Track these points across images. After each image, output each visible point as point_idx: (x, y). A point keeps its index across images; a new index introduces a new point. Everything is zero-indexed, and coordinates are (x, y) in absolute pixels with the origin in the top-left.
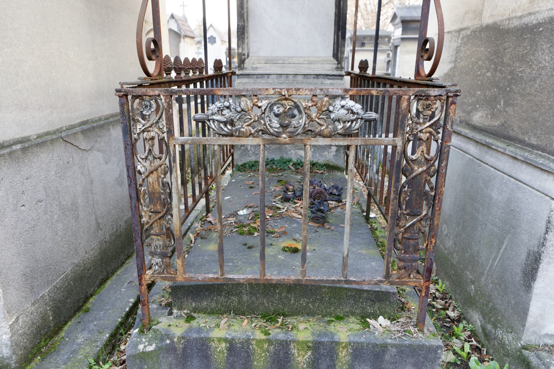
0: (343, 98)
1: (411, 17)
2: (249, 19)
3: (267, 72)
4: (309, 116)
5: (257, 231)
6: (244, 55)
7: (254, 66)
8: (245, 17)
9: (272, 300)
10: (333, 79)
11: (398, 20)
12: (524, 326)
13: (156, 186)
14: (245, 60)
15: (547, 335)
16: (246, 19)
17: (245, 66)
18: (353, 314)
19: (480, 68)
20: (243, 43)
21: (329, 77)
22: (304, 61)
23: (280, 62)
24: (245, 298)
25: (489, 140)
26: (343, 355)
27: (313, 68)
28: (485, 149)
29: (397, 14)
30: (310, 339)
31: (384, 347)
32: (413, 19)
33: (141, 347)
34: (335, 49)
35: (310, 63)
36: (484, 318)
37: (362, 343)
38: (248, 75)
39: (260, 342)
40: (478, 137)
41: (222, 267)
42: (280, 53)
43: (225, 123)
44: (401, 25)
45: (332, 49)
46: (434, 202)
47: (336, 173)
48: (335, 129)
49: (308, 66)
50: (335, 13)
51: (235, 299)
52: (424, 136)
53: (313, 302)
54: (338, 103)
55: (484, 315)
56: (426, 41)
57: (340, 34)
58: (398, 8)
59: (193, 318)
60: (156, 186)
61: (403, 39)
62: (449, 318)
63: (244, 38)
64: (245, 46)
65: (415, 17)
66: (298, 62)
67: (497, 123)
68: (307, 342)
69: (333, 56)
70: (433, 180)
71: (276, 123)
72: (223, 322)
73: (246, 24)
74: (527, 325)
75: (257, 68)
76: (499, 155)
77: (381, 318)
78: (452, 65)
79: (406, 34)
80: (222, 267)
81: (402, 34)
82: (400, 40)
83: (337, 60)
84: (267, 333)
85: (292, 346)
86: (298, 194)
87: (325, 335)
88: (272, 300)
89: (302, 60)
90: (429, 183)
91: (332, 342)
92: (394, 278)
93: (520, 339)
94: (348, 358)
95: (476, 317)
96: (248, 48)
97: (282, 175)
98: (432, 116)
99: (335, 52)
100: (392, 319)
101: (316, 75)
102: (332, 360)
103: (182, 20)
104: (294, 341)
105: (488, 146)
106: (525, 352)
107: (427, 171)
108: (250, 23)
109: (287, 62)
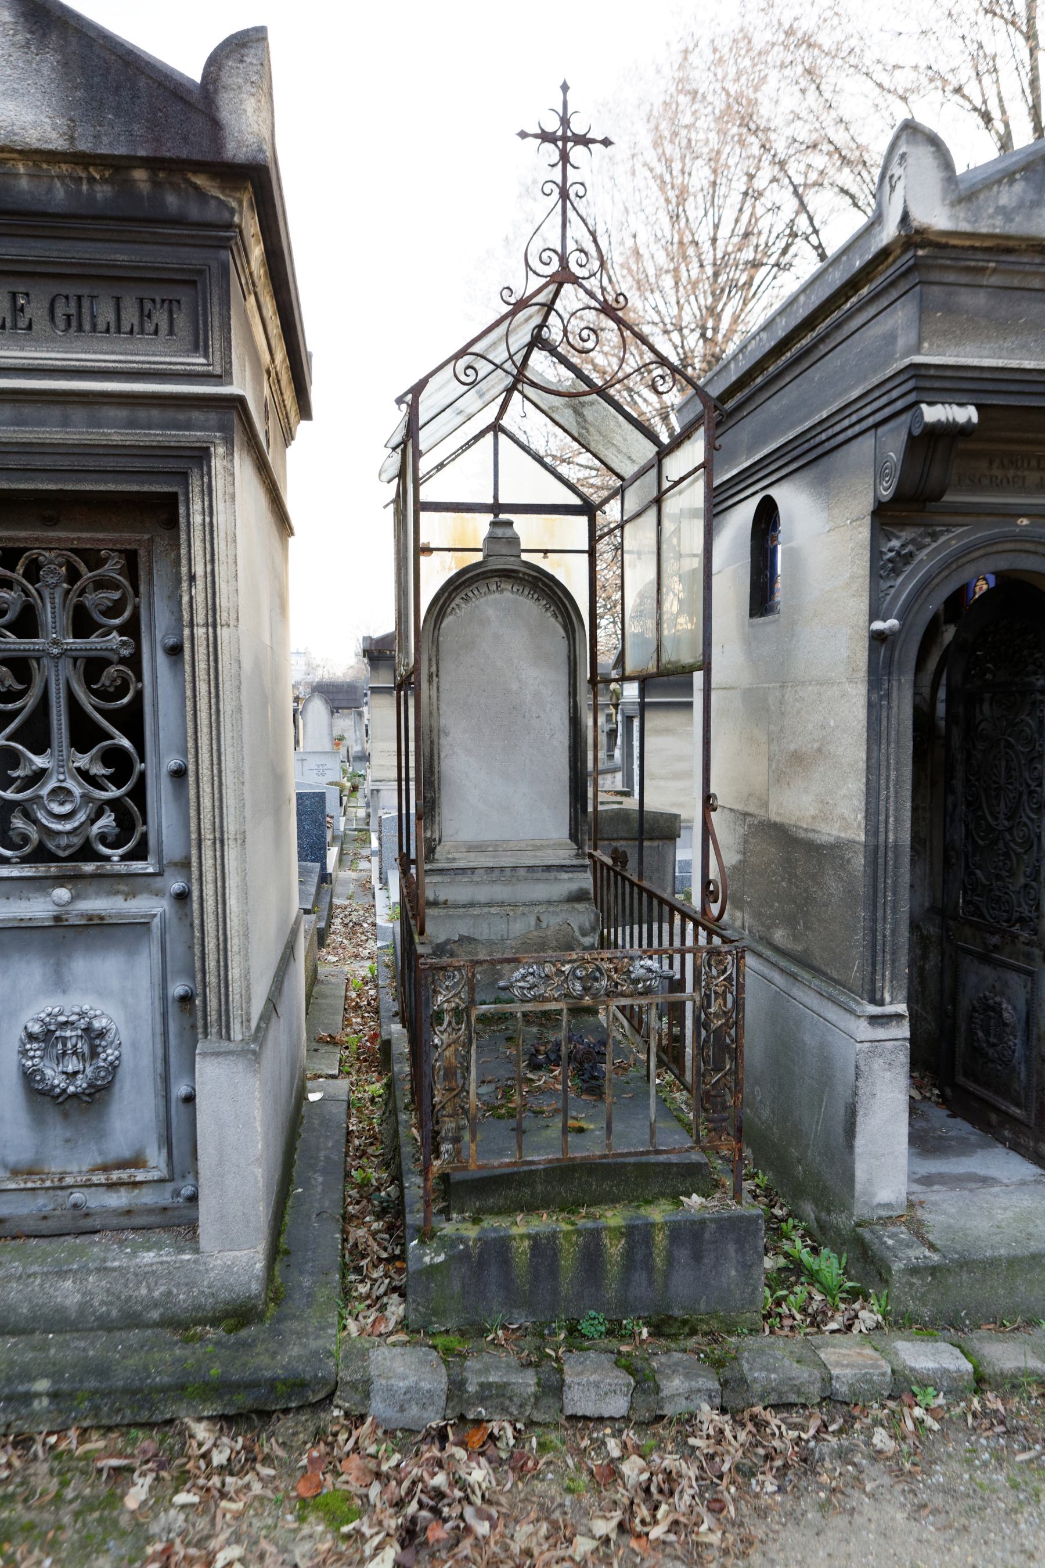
0: (641, 958)
3: (471, 865)
4: (609, 977)
5: (510, 1115)
9: (574, 1183)
12: (853, 1197)
13: (453, 1060)
15: (879, 1205)
18: (663, 1195)
19: (774, 873)
24: (539, 1188)
25: (794, 969)
26: (660, 1238)
28: (791, 979)
30: (623, 1223)
31: (703, 1222)
33: (427, 1259)
35: (537, 848)
36: (817, 1206)
37: (679, 1222)
39: (567, 1234)
40: (783, 963)
41: (520, 1148)
43: (530, 989)
46: (736, 1054)
47: (586, 1018)
48: (636, 989)
51: (527, 1191)
52: (720, 990)
53: (618, 1186)
54: (638, 963)
55: (816, 1202)
56: (709, 882)
59: (481, 1220)
60: (453, 1060)
62: (776, 1217)
64: (436, 827)
67: (799, 948)
68: (620, 1227)
70: (733, 1032)
71: (578, 986)
72: (518, 1219)
74: (856, 1195)
76: (806, 989)
77: (694, 1196)
78: (739, 857)
80: (520, 1148)
83: (577, 843)
84: (573, 1224)
85: (603, 1235)
86: (553, 1057)
87: (638, 1218)
88: (574, 1183)
89: (523, 845)
90: (730, 1035)
91: (647, 1225)
92: (705, 1142)
93: (852, 1215)
94: (665, 1242)
95: (808, 1209)
96: (440, 830)
97: (507, 1029)
98: (724, 971)
100: (706, 1195)
102: (649, 1247)
104: (606, 1228)
105: (793, 976)
106: (859, 1230)
107: (726, 1024)
108: (443, 793)
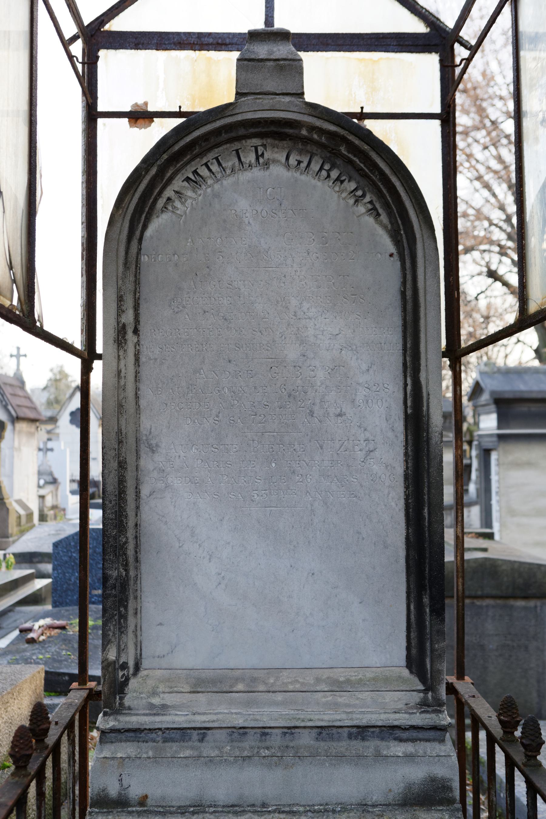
1: (514, 392)
2: (143, 556)
6: (124, 666)
7: (156, 701)
8: (130, 552)
10: (413, 740)
11: (485, 397)
14: (127, 680)
16: (131, 559)
17: (127, 702)
20: (122, 630)
21: (398, 733)
22: (318, 680)
23: (240, 687)
27: (348, 705)
29: (482, 384)
32: (518, 396)
34: (414, 643)
35: (338, 687)
38: (136, 734)
42: (239, 658)
44: (493, 407)
45: (404, 644)
49: (330, 698)
50: (407, 538)
57: (426, 600)
58: (481, 373)
61: (501, 437)
63: (124, 617)
65: (522, 392)
66: (298, 686)
69: (409, 666)
73: (132, 573)
75: (164, 707)
79: (508, 428)
81: (499, 427)
82: (495, 439)
96: (138, 646)
99: (414, 651)
101: (358, 727)
103: (11, 385)
108: (144, 567)
109: (262, 688)
